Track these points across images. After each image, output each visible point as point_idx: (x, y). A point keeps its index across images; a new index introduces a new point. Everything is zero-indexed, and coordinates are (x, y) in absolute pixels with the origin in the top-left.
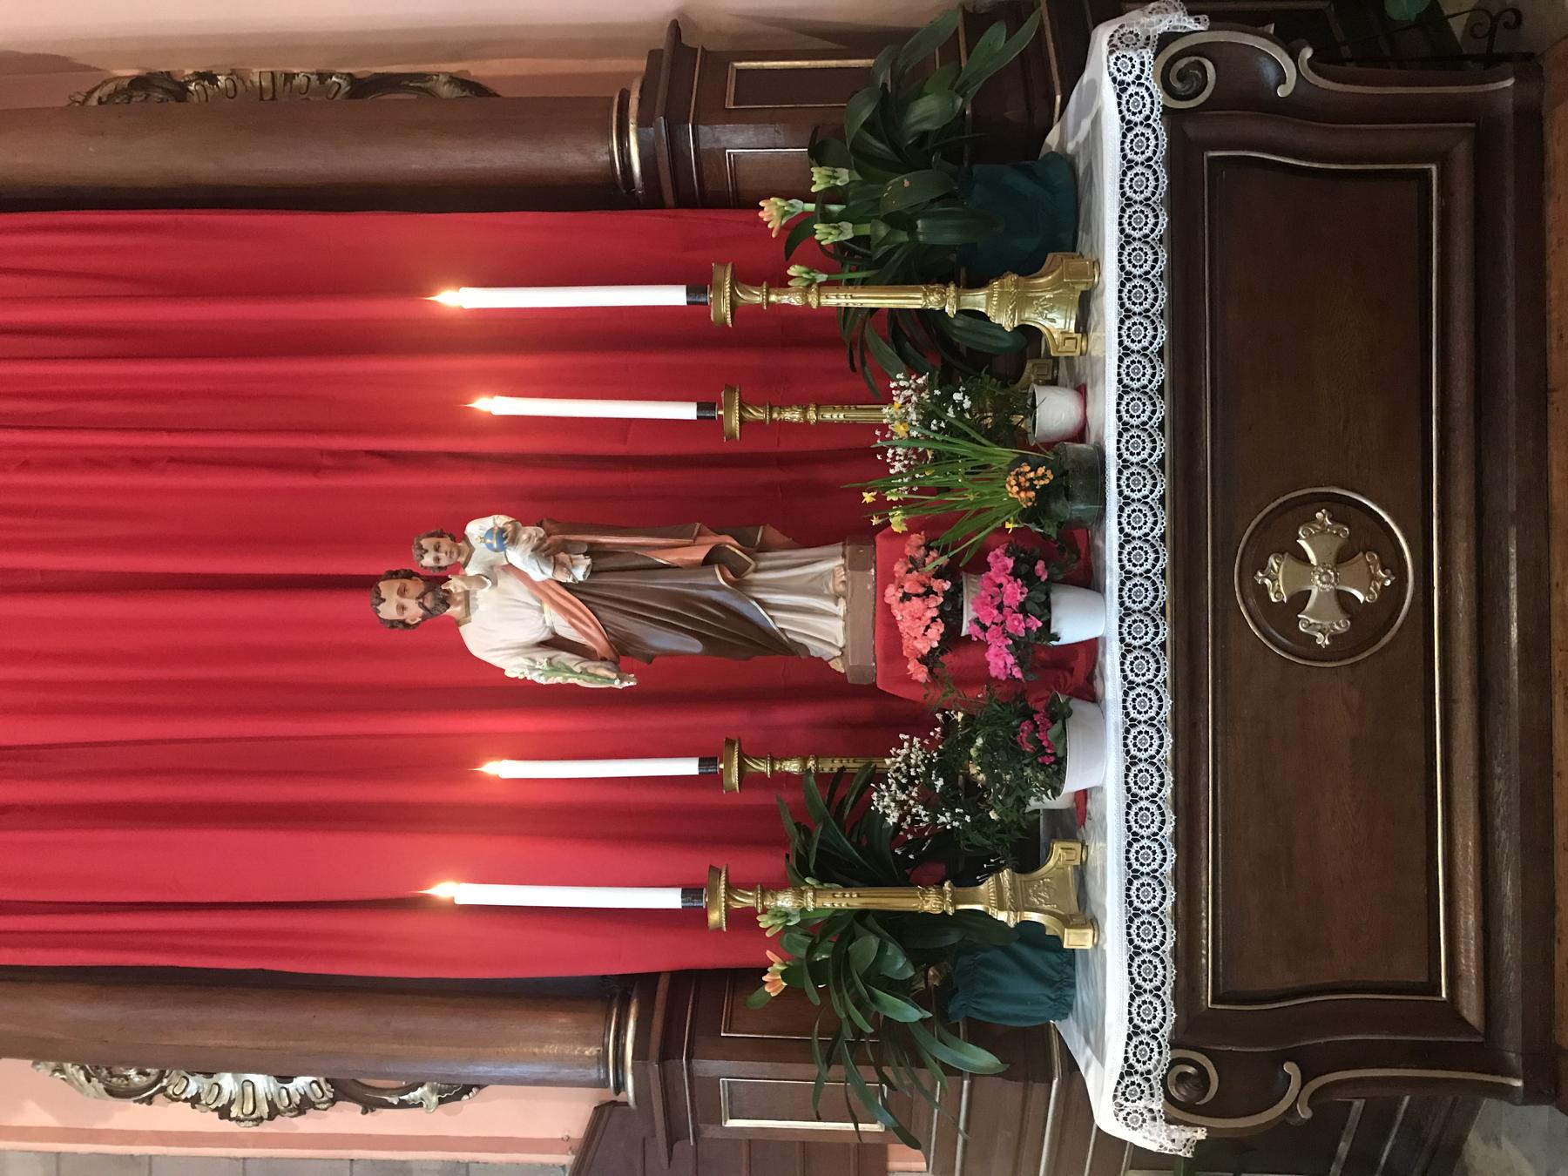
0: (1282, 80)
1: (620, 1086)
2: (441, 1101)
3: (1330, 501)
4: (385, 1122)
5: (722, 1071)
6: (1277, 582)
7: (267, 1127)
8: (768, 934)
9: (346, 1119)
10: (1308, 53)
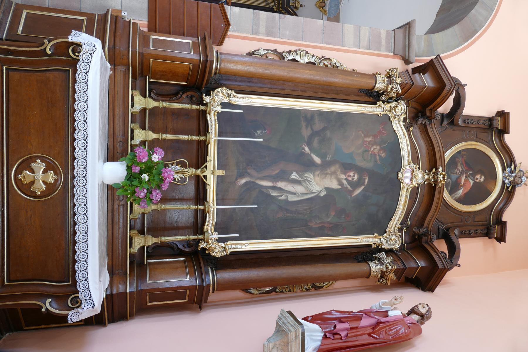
0: (50, 303)
1: (217, 52)
2: (259, 50)
3: (36, 197)
4: (272, 47)
5: (191, 55)
6: (51, 177)
7: (297, 48)
8: (181, 93)
9: (281, 48)
10: (43, 310)
